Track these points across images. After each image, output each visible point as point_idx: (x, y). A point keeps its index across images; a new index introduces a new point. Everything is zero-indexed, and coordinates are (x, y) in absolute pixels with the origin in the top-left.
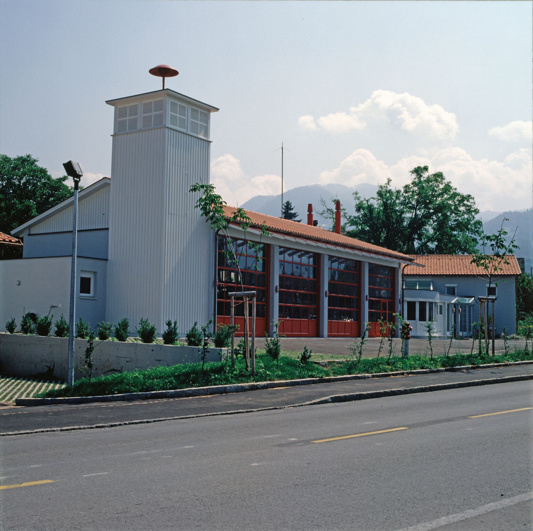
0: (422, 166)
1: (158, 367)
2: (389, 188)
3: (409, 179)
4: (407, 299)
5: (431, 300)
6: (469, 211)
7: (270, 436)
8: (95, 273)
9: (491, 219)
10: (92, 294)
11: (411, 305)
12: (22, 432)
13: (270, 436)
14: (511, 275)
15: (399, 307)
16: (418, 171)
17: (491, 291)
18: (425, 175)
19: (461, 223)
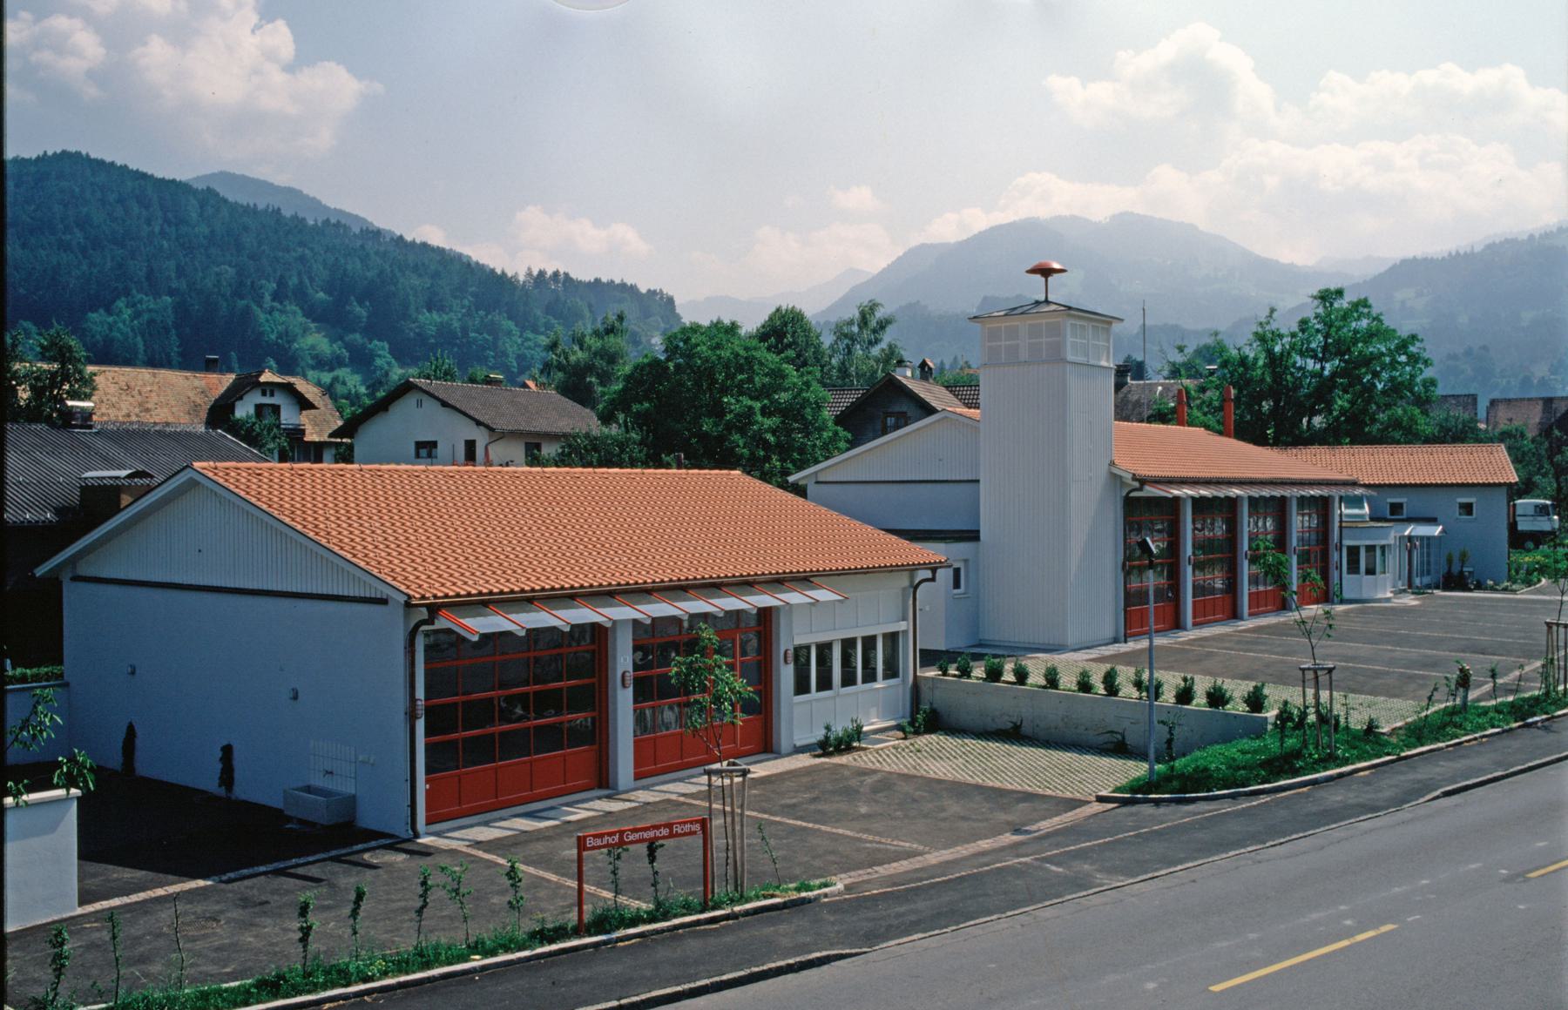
0: (1333, 287)
1: (731, 667)
2: (1274, 326)
3: (1312, 310)
4: (1347, 542)
5: (1383, 542)
6: (1414, 359)
7: (553, 877)
8: (966, 561)
9: (1419, 255)
10: (962, 590)
11: (1354, 552)
12: (311, 859)
13: (553, 877)
14: (1500, 485)
15: (1336, 556)
16: (1326, 297)
17: (1467, 509)
18: (1343, 304)
19: (1401, 383)
